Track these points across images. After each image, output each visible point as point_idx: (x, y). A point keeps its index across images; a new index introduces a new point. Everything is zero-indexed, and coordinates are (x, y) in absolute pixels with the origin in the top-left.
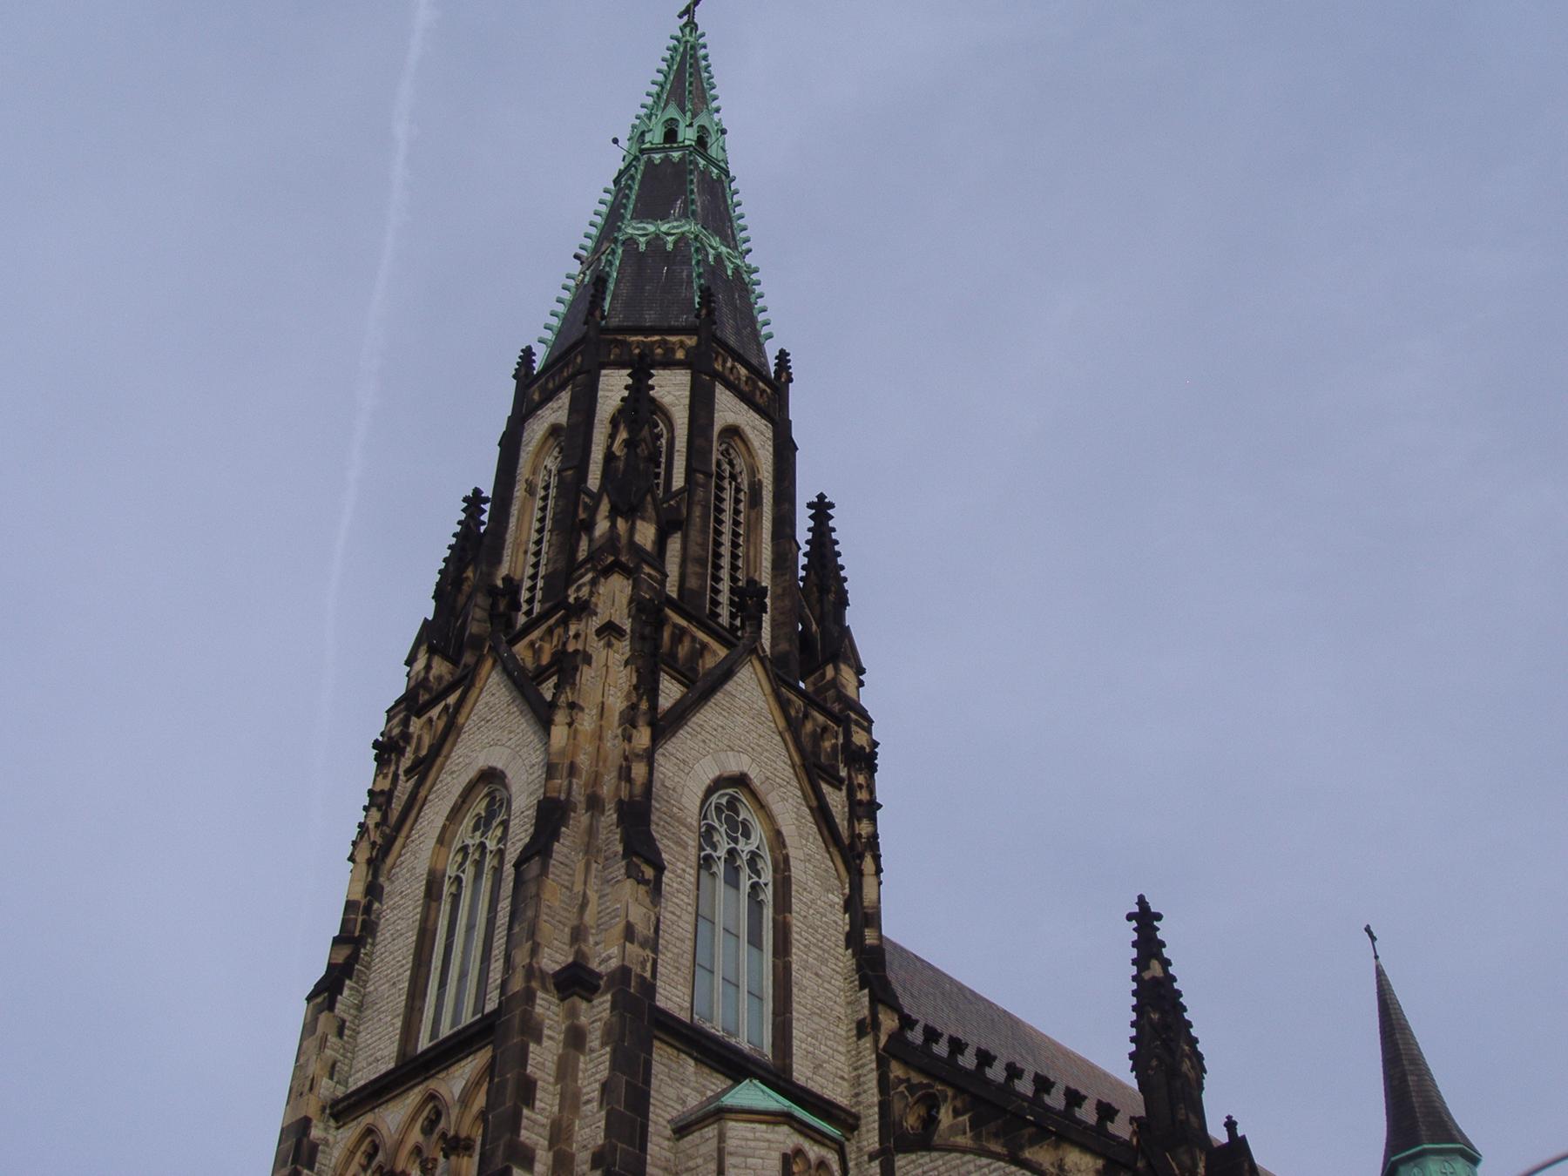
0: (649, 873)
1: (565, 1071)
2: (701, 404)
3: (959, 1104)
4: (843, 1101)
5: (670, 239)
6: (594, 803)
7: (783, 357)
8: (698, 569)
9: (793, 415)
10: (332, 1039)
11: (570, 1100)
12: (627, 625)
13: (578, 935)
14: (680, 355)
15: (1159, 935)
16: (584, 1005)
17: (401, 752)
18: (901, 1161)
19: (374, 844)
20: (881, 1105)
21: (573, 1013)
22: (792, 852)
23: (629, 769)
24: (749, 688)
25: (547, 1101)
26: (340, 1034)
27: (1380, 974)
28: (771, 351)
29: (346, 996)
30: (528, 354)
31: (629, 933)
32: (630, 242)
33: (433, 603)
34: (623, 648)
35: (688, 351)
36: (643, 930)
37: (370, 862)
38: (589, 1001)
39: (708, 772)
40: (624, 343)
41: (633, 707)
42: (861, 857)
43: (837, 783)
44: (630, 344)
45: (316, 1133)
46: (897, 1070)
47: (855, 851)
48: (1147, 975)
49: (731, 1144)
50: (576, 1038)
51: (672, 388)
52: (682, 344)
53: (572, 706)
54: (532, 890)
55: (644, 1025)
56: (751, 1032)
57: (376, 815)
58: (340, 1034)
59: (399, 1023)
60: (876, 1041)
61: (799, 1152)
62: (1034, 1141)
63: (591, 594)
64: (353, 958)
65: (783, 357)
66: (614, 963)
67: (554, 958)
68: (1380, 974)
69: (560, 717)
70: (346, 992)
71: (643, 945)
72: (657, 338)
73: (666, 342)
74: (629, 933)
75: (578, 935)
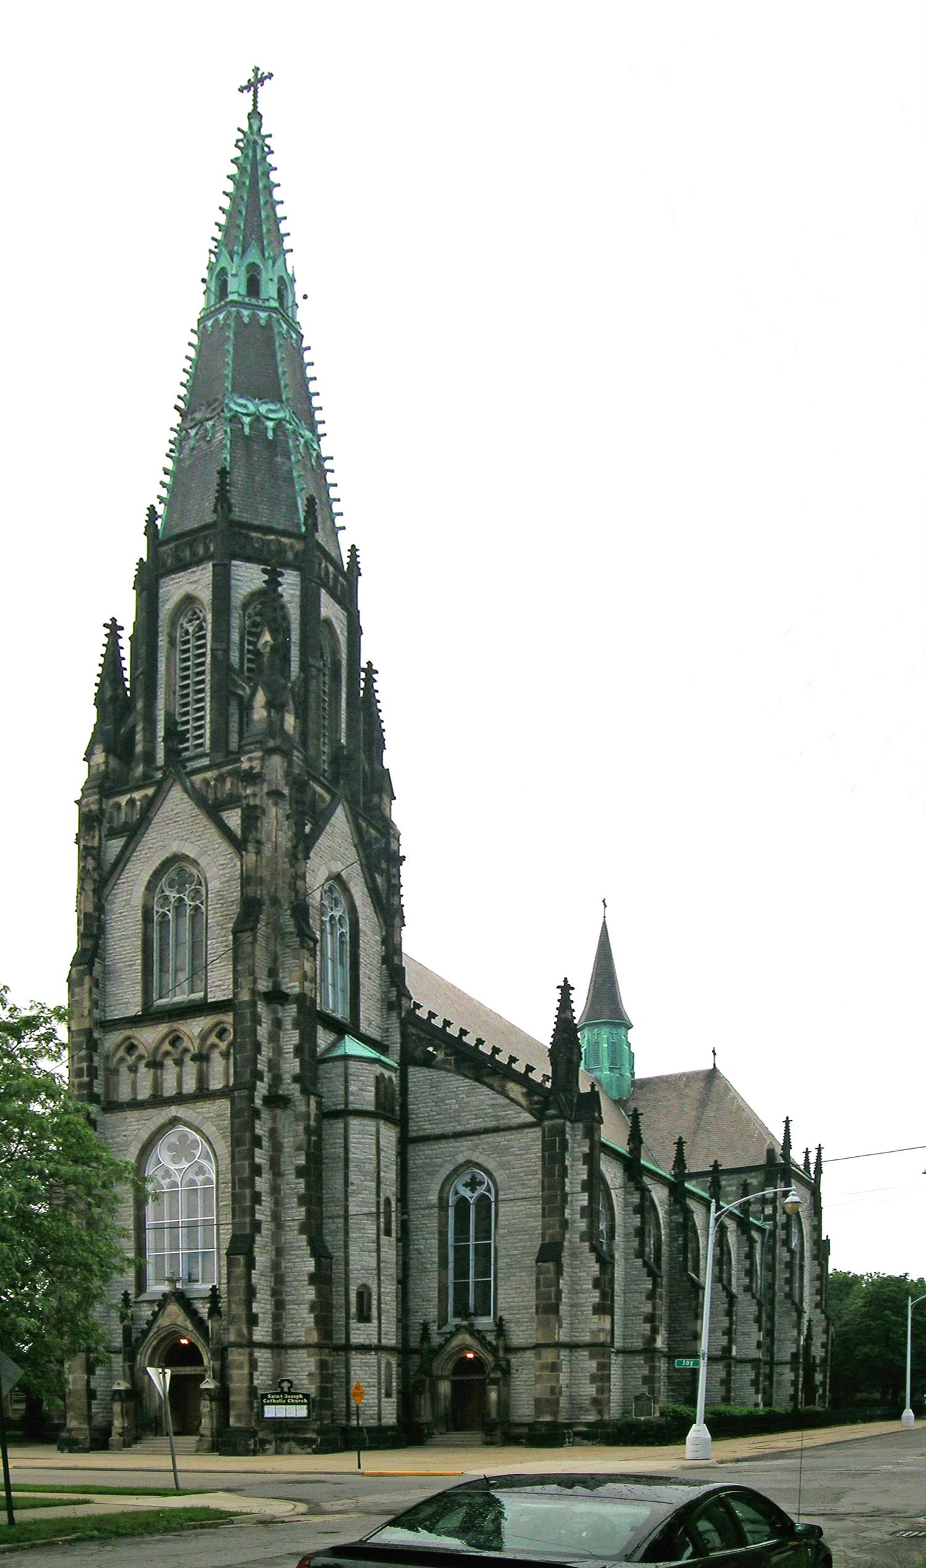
0: (311, 944)
1: (274, 1037)
2: (309, 604)
3: (449, 1051)
4: (379, 1038)
5: (270, 424)
6: (275, 902)
7: (353, 550)
8: (315, 742)
9: (361, 606)
10: (94, 990)
11: (278, 1051)
12: (286, 791)
13: (273, 973)
14: (290, 556)
15: (571, 998)
16: (280, 1008)
17: (100, 823)
18: (411, 1070)
19: (95, 881)
20: (402, 1044)
21: (275, 1011)
22: (360, 915)
23: (295, 884)
24: (177, 800)
25: (266, 1052)
26: (97, 986)
27: (604, 925)
28: (345, 542)
29: (97, 967)
30: (152, 512)
31: (305, 977)
32: (235, 418)
33: (94, 710)
34: (286, 807)
35: (296, 555)
36: (310, 974)
37: (94, 891)
38: (282, 1005)
39: (323, 875)
40: (247, 537)
41: (295, 847)
42: (393, 917)
43: (381, 873)
44: (252, 538)
45: (96, 1035)
46: (412, 1030)
47: (390, 913)
48: (563, 1016)
49: (351, 1071)
50: (278, 1024)
51: (290, 585)
52: (292, 547)
53: (259, 842)
54: (248, 948)
55: (312, 1017)
56: (341, 1013)
57: (91, 864)
58: (97, 986)
59: (139, 987)
60: (400, 1014)
61: (382, 1074)
62: (488, 1075)
63: (262, 768)
64: (96, 946)
65: (353, 550)
66: (297, 990)
67: (263, 985)
68: (604, 925)
69: (251, 847)
70: (96, 965)
71: (311, 982)
72: (272, 537)
73: (279, 542)
74: (305, 977)
75: (273, 973)
